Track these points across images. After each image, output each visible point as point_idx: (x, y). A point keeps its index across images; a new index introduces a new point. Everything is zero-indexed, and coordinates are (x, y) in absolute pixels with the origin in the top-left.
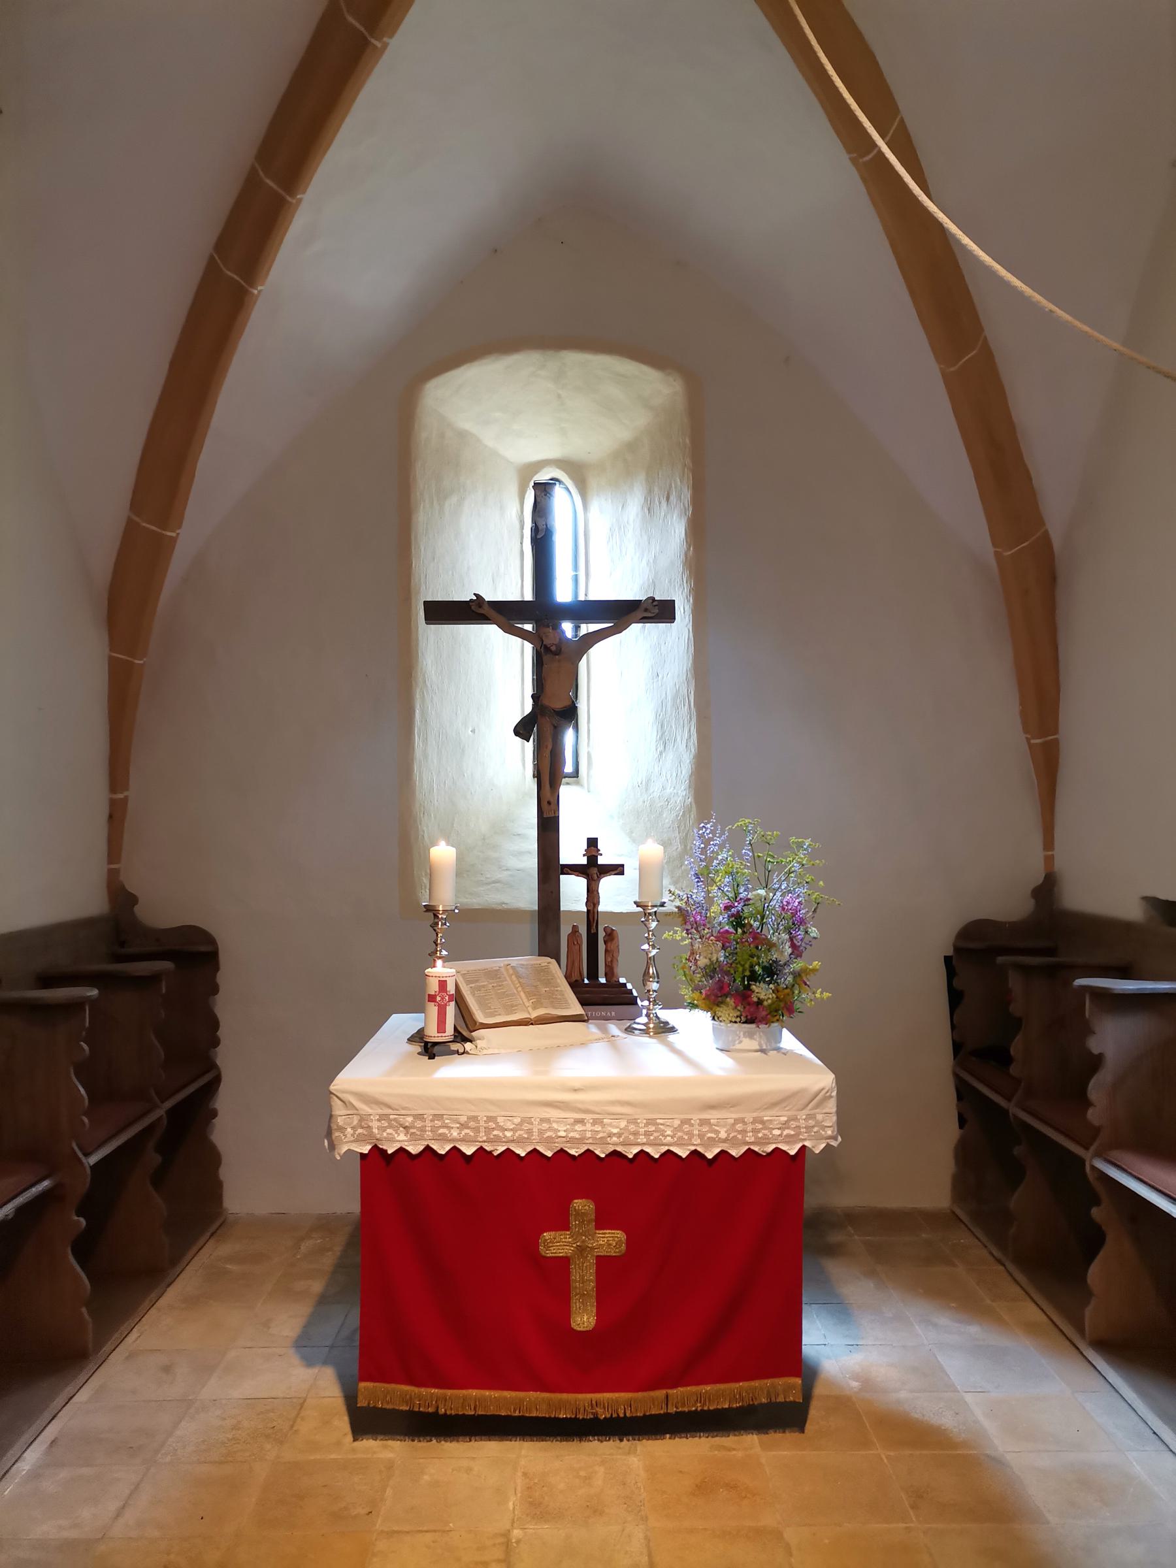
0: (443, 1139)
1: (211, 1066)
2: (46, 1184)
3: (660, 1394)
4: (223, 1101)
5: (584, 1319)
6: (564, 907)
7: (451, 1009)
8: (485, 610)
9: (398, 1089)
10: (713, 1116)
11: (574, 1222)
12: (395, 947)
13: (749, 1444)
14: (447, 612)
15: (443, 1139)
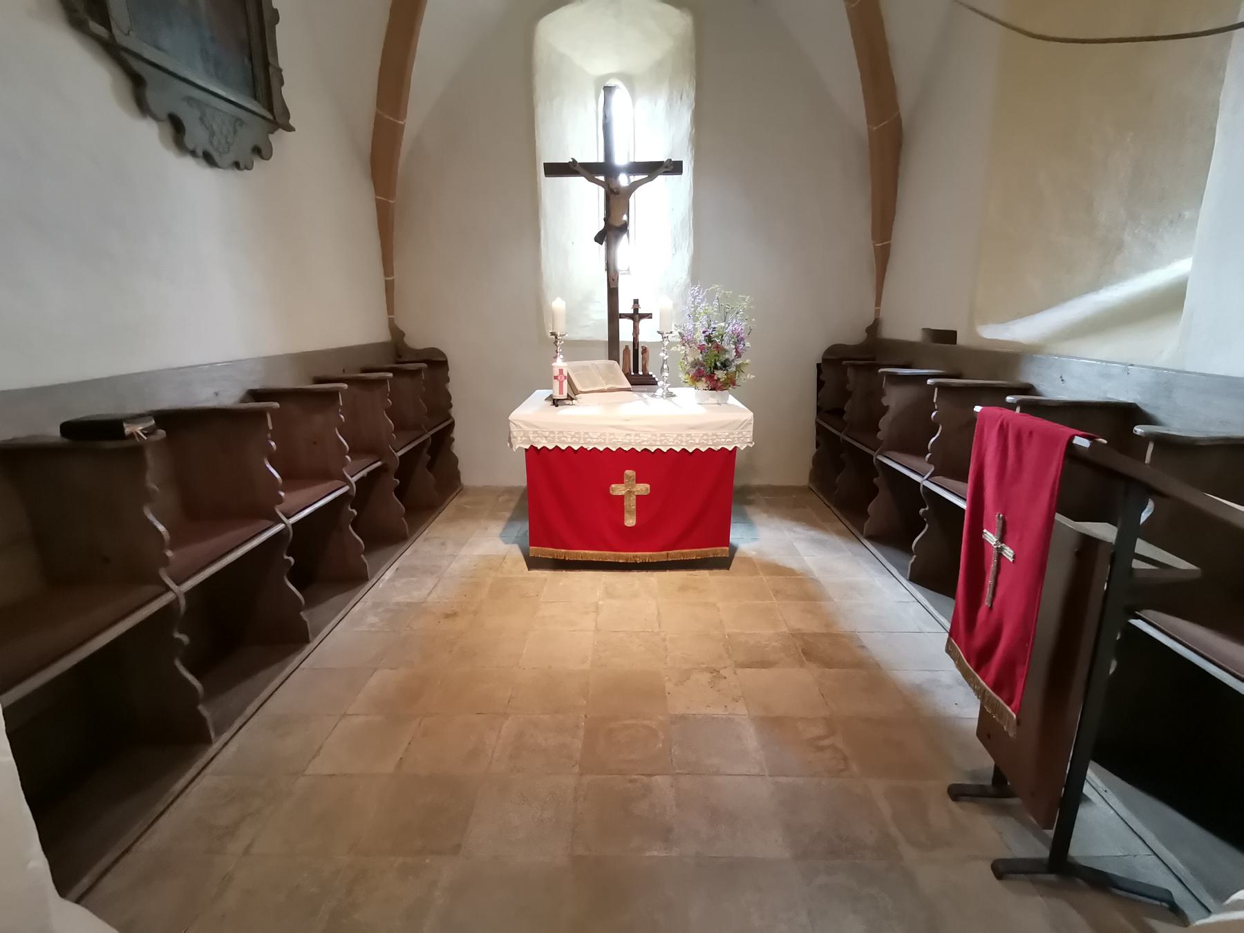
0: (564, 442)
1: (449, 417)
2: (379, 463)
3: (664, 553)
4: (457, 433)
5: (630, 521)
6: (621, 339)
7: (565, 383)
8: (578, 168)
9: (538, 422)
10: (692, 432)
11: (626, 480)
12: (535, 354)
13: (703, 574)
14: (555, 170)
15: (564, 442)
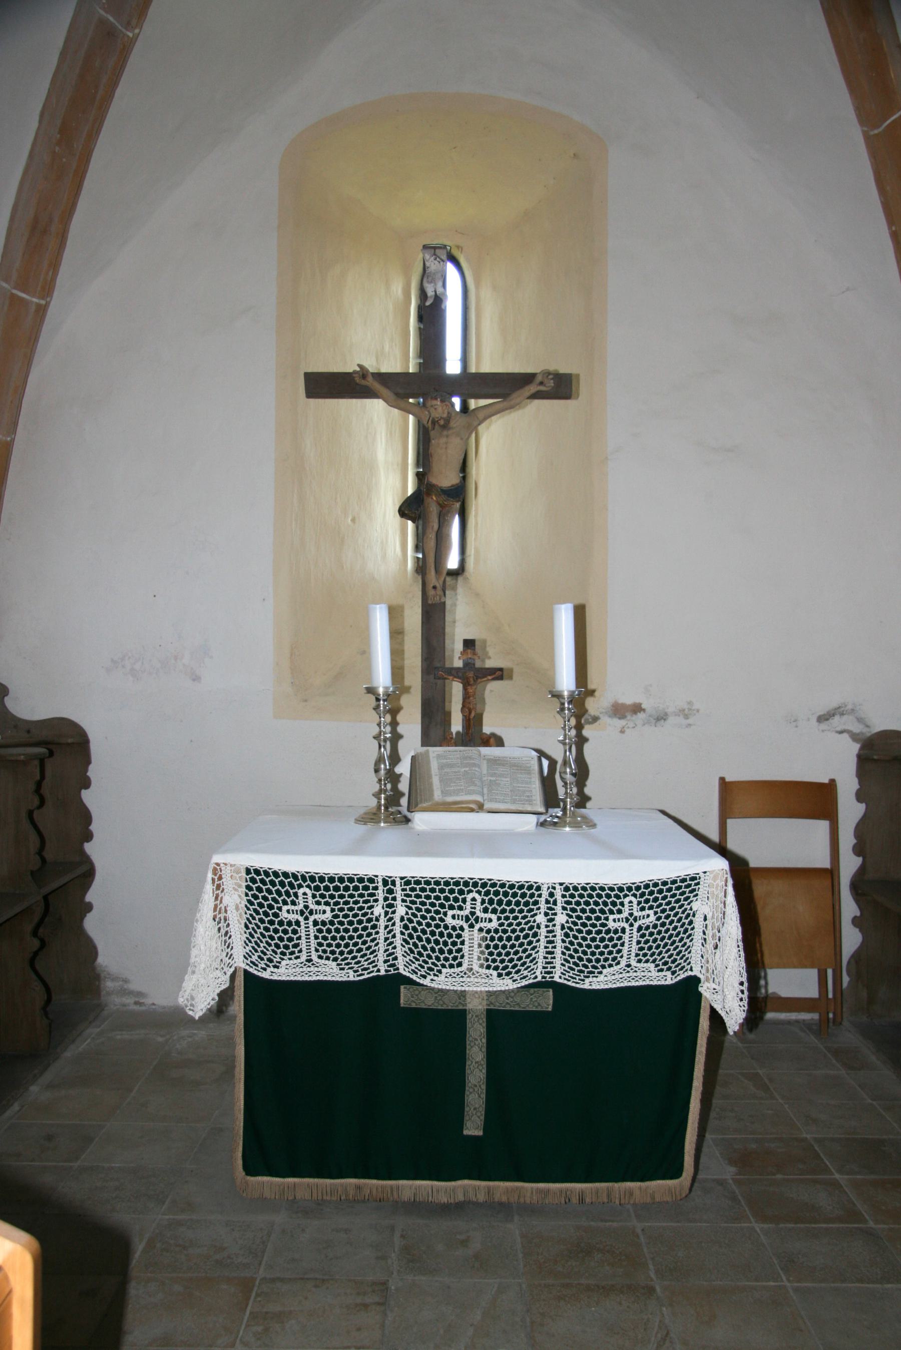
8: (370, 382)
